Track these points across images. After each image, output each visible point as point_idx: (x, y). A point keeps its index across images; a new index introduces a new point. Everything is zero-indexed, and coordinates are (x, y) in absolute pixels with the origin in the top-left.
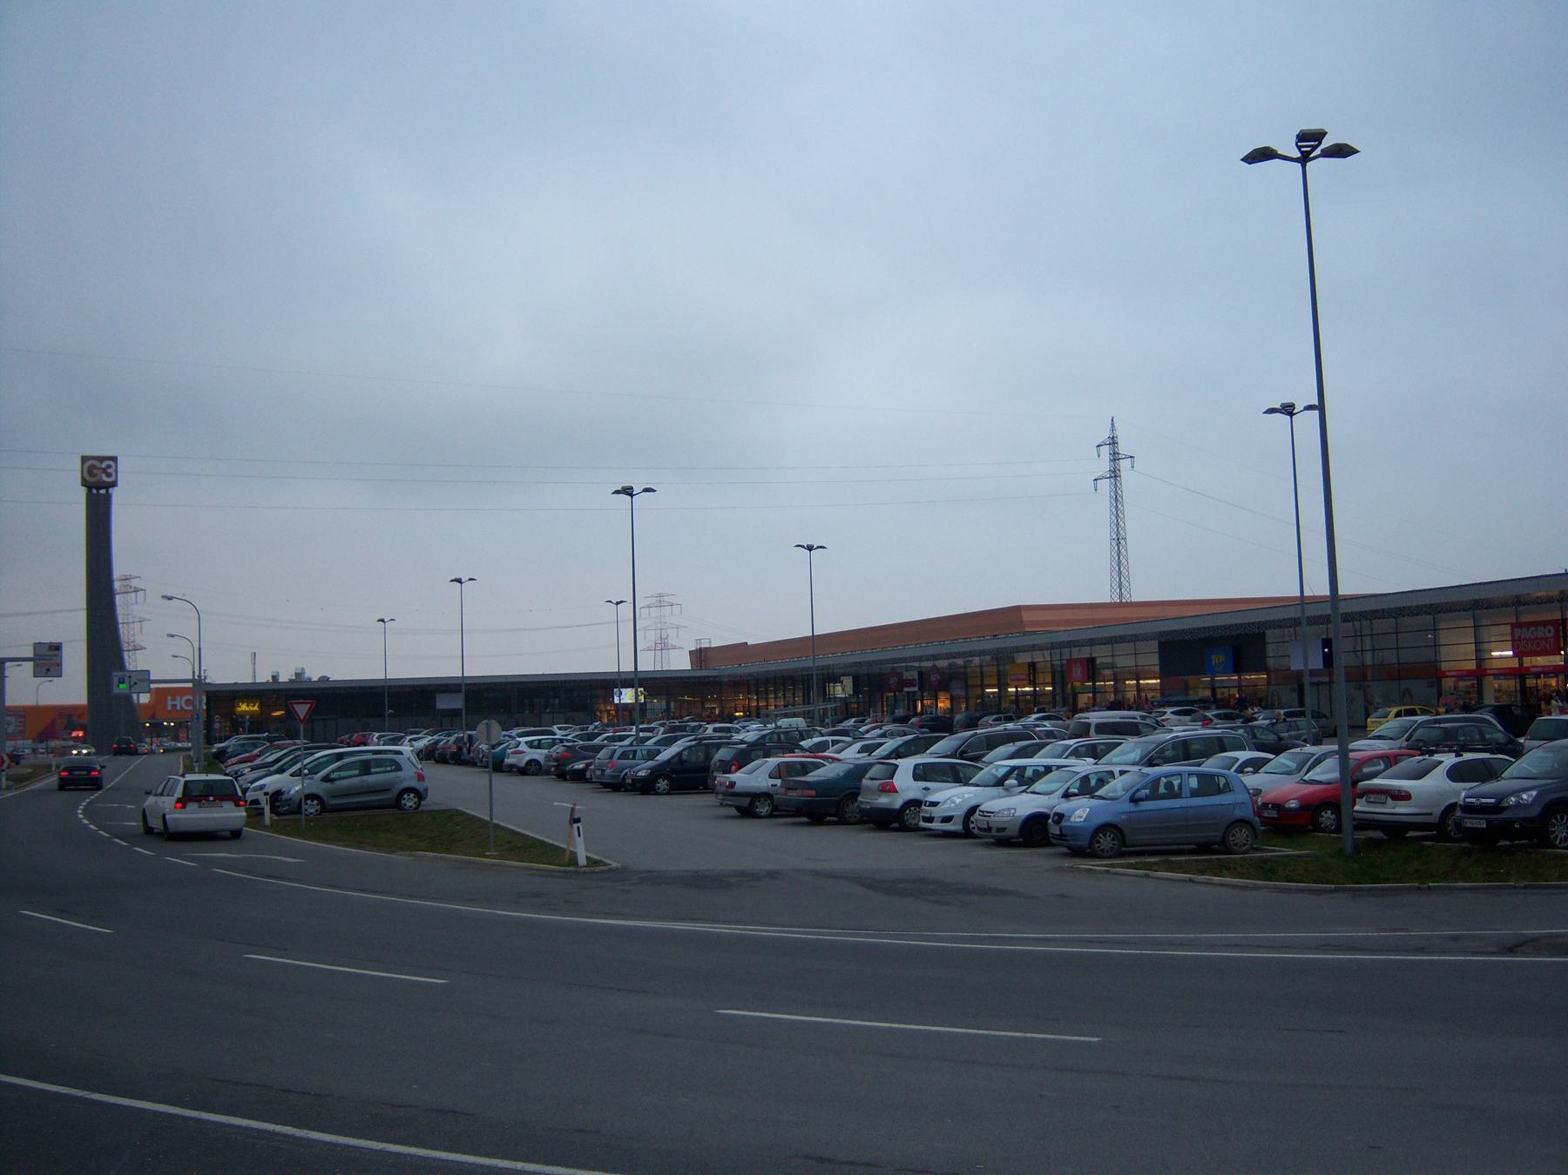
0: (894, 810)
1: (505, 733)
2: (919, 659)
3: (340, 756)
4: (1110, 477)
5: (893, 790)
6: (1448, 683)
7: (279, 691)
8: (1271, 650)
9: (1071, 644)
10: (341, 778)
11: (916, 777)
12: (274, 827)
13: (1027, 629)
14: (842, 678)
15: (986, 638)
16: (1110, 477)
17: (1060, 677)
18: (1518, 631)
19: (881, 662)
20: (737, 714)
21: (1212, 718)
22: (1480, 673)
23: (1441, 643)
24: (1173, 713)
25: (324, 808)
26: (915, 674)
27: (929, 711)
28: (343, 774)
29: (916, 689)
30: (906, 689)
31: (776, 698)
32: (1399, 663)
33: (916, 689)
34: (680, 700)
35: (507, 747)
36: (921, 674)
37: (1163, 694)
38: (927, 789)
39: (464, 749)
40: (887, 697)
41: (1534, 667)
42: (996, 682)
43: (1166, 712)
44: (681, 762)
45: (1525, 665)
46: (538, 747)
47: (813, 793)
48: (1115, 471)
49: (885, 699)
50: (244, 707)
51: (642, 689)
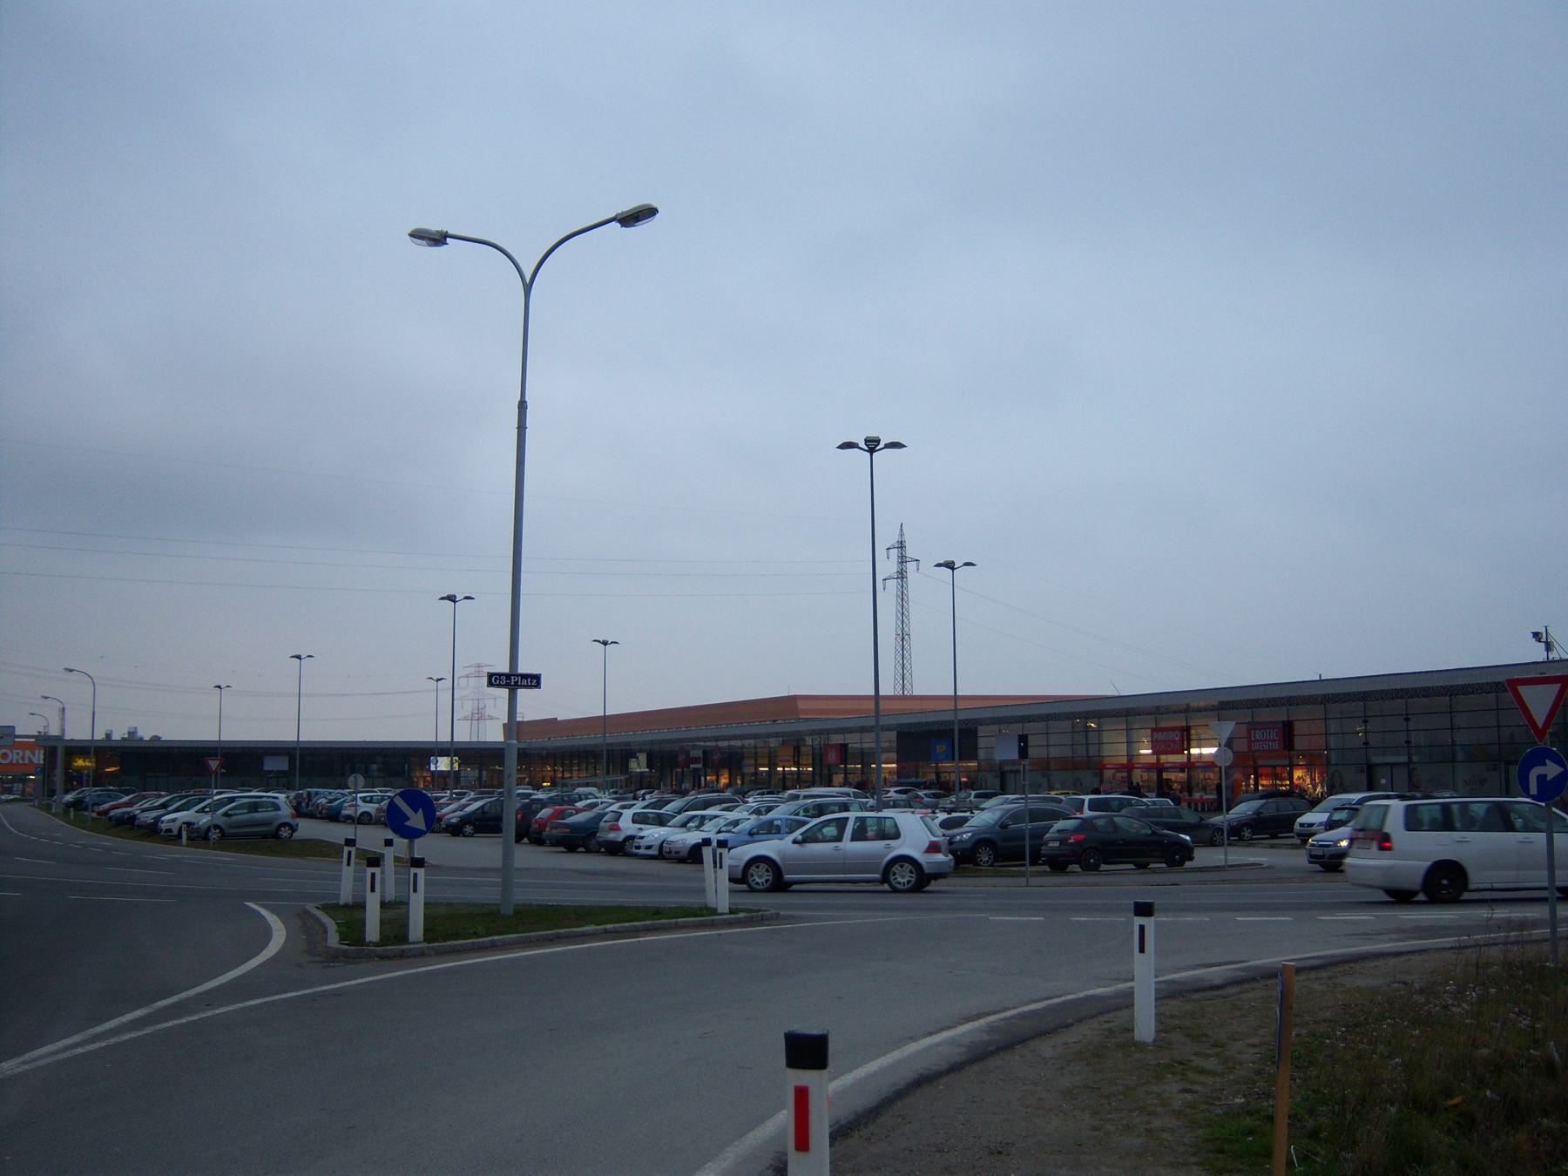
0: (618, 842)
1: (406, 774)
2: (707, 739)
3: (232, 800)
4: (897, 578)
5: (618, 829)
6: (1108, 774)
7: (110, 748)
8: (981, 742)
9: (829, 732)
10: (235, 815)
11: (634, 821)
12: (188, 846)
13: (801, 717)
14: (638, 754)
15: (779, 722)
16: (897, 578)
17: (818, 759)
18: (1155, 733)
19: (670, 741)
20: (545, 784)
21: (923, 796)
22: (1130, 767)
23: (1105, 741)
24: (896, 792)
25: (224, 835)
26: (700, 753)
27: (711, 785)
28: (237, 812)
29: (700, 766)
30: (692, 766)
31: (579, 770)
32: (1088, 757)
33: (700, 766)
34: (492, 770)
35: (344, 801)
36: (705, 752)
37: (898, 777)
38: (641, 829)
39: (303, 804)
40: (677, 772)
41: (1167, 763)
42: (767, 762)
43: (889, 791)
44: (483, 813)
45: (1161, 761)
46: (370, 802)
47: (568, 830)
48: (902, 573)
49: (674, 773)
50: (80, 762)
51: (457, 758)
